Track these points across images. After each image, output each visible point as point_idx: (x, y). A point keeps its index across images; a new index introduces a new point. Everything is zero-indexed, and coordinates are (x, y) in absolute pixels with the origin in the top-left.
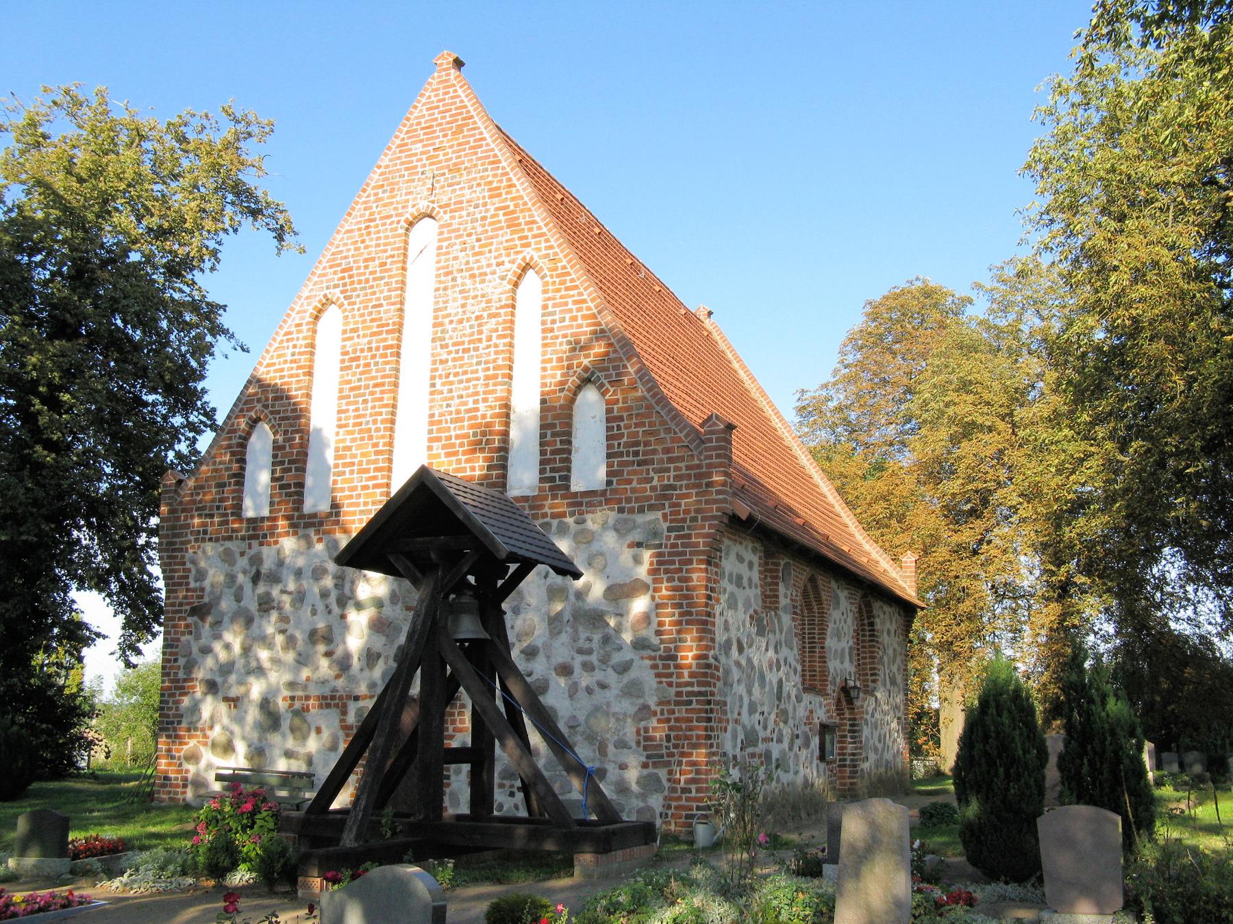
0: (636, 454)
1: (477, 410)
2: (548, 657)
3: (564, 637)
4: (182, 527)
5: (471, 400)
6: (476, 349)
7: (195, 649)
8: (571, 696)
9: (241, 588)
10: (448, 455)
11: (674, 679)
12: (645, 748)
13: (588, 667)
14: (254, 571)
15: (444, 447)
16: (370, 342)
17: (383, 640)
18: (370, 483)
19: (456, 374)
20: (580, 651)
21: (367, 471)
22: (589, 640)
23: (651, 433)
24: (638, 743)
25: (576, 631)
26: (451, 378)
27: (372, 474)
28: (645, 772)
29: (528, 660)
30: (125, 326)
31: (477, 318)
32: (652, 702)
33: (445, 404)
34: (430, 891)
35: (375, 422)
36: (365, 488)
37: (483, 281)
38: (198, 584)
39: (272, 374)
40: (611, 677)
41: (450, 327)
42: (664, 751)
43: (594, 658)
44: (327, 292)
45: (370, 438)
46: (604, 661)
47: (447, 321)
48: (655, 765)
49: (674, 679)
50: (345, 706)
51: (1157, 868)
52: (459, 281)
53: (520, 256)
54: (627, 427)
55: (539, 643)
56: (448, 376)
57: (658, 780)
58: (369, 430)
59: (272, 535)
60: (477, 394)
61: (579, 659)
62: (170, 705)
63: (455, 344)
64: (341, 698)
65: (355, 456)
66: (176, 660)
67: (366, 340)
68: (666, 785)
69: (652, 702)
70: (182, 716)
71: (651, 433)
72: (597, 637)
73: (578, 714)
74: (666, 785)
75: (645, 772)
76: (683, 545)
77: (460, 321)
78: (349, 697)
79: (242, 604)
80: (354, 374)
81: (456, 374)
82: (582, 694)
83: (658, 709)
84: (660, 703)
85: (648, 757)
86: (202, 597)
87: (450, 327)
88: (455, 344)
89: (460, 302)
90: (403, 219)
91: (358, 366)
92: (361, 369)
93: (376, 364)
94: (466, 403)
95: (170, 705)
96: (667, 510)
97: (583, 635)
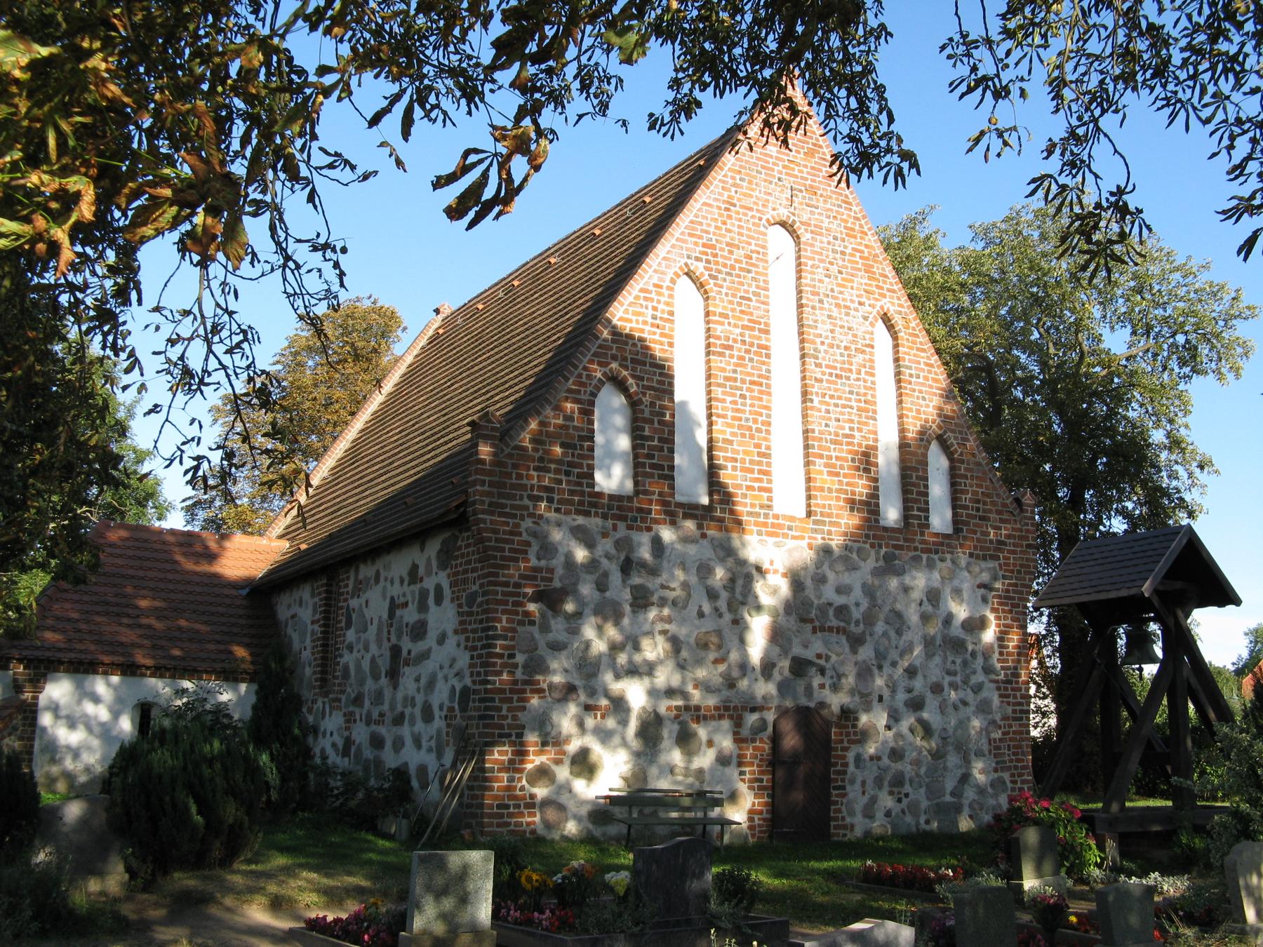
0: (978, 510)
1: (852, 436)
2: (925, 677)
3: (937, 659)
4: (513, 486)
5: (847, 425)
6: (848, 378)
7: (542, 644)
8: (942, 712)
9: (606, 575)
10: (830, 473)
11: (1011, 700)
12: (995, 755)
13: (953, 686)
14: (623, 558)
15: (826, 465)
16: (742, 335)
17: (777, 649)
18: (756, 485)
19: (832, 397)
20: (949, 673)
21: (752, 471)
22: (954, 662)
23: (988, 495)
24: (990, 752)
25: (946, 657)
26: (827, 399)
27: (756, 476)
28: (996, 775)
29: (910, 678)
30: (90, 110)
31: (846, 348)
32: (998, 717)
33: (824, 423)
34: (219, 921)
35: (755, 421)
36: (749, 488)
37: (847, 314)
38: (543, 563)
39: (657, 337)
40: (970, 697)
41: (822, 348)
42: (1007, 758)
43: (958, 679)
44: (689, 262)
45: (752, 437)
46: (965, 682)
47: (818, 340)
48: (1003, 769)
49: (1011, 700)
50: (740, 717)
51: (231, 826)
52: (826, 305)
53: (879, 304)
54: (971, 486)
55: (917, 663)
56: (824, 395)
57: (1004, 782)
58: (750, 429)
59: (644, 520)
60: (852, 421)
61: (948, 679)
62: (504, 712)
63: (828, 366)
64: (735, 708)
65: (737, 452)
66: (512, 656)
67: (738, 331)
68: (1009, 785)
69: (998, 717)
70: (524, 727)
71: (988, 495)
72: (958, 661)
73: (947, 726)
74: (1009, 785)
75: (996, 775)
76: (1014, 592)
77: (831, 346)
78: (744, 709)
79: (608, 594)
80: (728, 363)
81: (832, 397)
82: (950, 710)
83: (1002, 723)
84: (1003, 719)
85: (997, 763)
86: (551, 580)
87: (822, 348)
88: (828, 366)
89: (829, 327)
90: (765, 218)
91: (732, 356)
92: (735, 360)
93: (751, 360)
94: (843, 428)
95: (504, 712)
96: (1002, 561)
97: (950, 659)
